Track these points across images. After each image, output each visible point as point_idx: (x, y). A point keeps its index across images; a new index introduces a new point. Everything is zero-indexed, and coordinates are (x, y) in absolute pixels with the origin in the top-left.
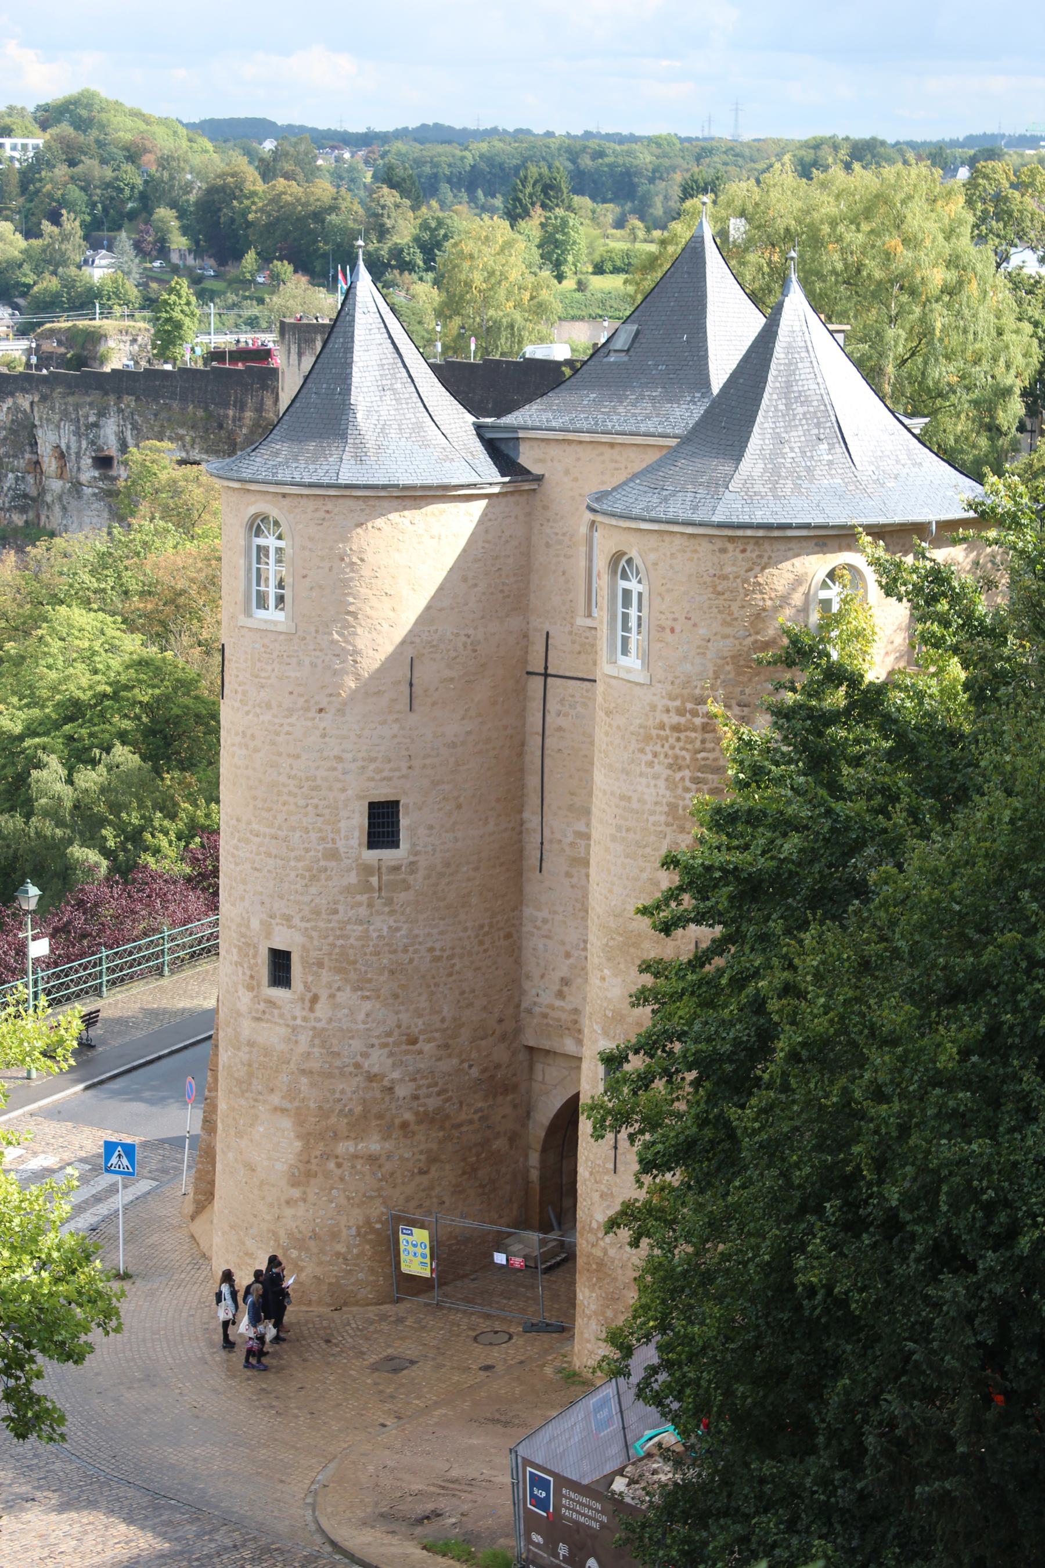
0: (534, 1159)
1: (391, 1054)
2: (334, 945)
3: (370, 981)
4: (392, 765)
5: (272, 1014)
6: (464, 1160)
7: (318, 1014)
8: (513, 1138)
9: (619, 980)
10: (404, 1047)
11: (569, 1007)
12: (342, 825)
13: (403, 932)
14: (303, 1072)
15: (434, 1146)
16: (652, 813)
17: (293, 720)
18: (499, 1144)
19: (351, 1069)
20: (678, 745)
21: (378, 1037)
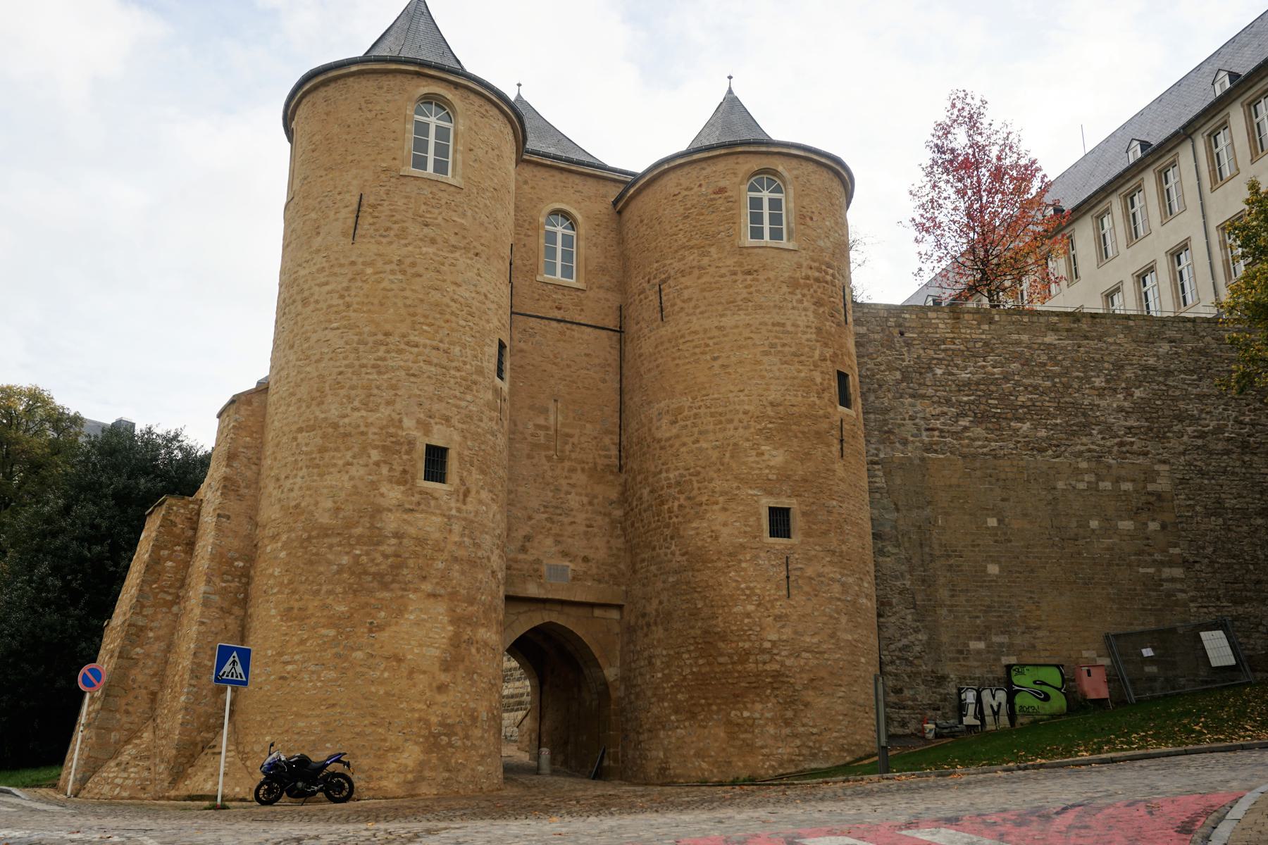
5: (428, 505)
11: (531, 558)
14: (456, 559)
16: (805, 333)
17: (457, 255)
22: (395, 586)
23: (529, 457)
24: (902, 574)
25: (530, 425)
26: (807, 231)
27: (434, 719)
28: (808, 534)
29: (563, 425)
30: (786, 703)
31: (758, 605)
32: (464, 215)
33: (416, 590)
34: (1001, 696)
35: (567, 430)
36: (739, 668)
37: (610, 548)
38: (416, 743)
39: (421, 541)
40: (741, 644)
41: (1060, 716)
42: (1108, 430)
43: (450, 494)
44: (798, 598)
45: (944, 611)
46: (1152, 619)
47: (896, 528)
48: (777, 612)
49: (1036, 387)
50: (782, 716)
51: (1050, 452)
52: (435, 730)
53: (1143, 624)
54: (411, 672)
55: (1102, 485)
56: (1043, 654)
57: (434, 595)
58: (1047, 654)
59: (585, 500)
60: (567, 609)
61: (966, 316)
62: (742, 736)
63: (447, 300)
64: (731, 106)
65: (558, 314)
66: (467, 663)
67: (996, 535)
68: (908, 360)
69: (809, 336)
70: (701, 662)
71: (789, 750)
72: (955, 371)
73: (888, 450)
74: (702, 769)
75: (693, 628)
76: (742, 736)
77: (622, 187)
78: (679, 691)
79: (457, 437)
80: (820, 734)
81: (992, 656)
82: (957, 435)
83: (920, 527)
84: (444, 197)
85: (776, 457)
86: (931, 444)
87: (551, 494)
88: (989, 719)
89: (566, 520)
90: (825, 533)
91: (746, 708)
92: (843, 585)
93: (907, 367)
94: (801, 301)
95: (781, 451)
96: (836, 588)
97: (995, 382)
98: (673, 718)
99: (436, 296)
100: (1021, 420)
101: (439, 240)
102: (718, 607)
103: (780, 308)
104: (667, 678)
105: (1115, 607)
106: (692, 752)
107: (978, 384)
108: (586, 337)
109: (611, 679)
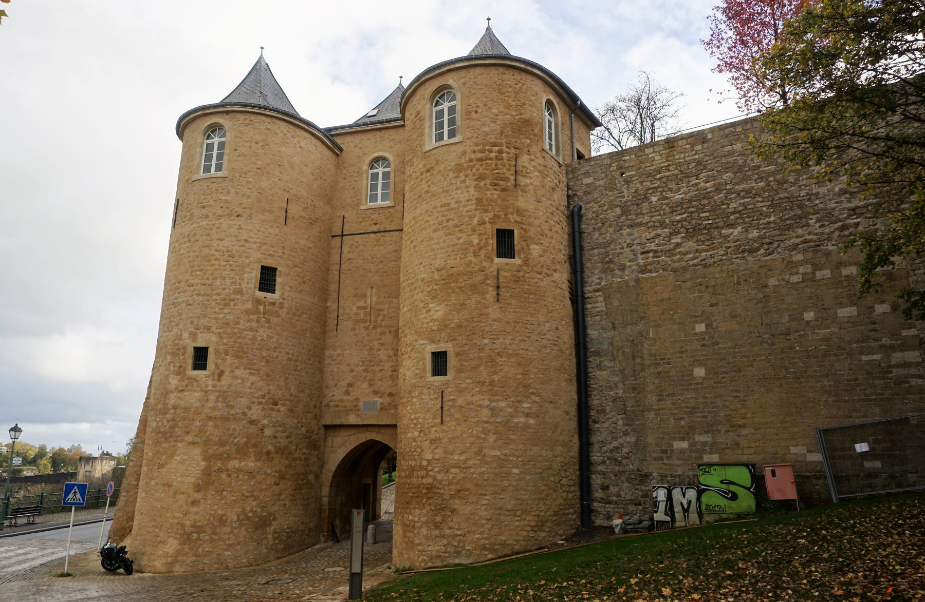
0: (325, 491)
1: (263, 410)
2: (235, 342)
3: (254, 364)
4: (274, 249)
6: (296, 481)
7: (223, 382)
8: (317, 477)
9: (443, 306)
10: (271, 406)
12: (246, 275)
13: (274, 340)
14: (210, 418)
15: (283, 469)
16: (465, 206)
17: (222, 221)
18: (311, 477)
19: (240, 416)
20: (481, 168)
21: (257, 398)
22: (172, 439)
23: (353, 329)
24: (616, 385)
25: (354, 308)
26: (472, 123)
27: (188, 523)
28: (459, 371)
29: (377, 303)
30: (436, 510)
31: (421, 432)
32: (228, 193)
33: (182, 441)
34: (692, 494)
35: (379, 307)
36: (409, 481)
38: (175, 538)
39: (186, 410)
41: (747, 515)
42: (828, 216)
43: (208, 376)
44: (450, 424)
45: (652, 415)
46: (877, 410)
47: (612, 344)
48: (432, 436)
49: (748, 192)
50: (433, 521)
51: (762, 251)
52: (188, 530)
53: (865, 416)
54: (175, 494)
55: (819, 274)
56: (747, 451)
57: (193, 443)
58: (752, 451)
59: (391, 353)
60: (383, 430)
61: (680, 143)
63: (213, 252)
64: (260, 73)
65: (375, 229)
66: (217, 485)
67: (704, 339)
68: (627, 195)
69: (469, 208)
71: (437, 548)
72: (669, 195)
73: (609, 277)
77: (335, 139)
79: (214, 339)
80: (464, 535)
81: (694, 455)
82: (670, 253)
83: (633, 341)
84: (215, 186)
85: (438, 311)
86: (645, 265)
87: (366, 353)
88: (679, 516)
89: (377, 369)
90: (475, 368)
91: (411, 513)
92: (492, 409)
93: (626, 202)
94: (464, 181)
95: (443, 306)
96: (485, 412)
97: (707, 196)
99: (206, 250)
100: (733, 226)
101: (210, 214)
103: (447, 191)
105: (831, 399)
107: (690, 201)
108: (394, 239)
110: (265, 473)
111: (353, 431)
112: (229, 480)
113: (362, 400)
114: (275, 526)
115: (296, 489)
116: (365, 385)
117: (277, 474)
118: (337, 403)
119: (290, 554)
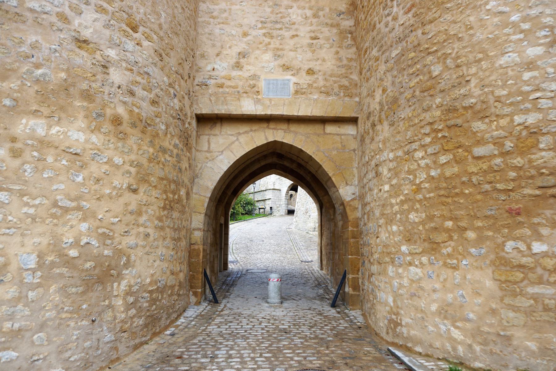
1: (107, 26)
6: (165, 192)
15: (145, 162)
36: (518, 161)
37: (340, 59)
40: (518, 119)
59: (309, 13)
60: (294, 127)
62: (531, 290)
70: (443, 159)
74: (452, 339)
75: (428, 109)
76: (531, 290)
78: (412, 209)
87: (269, 10)
89: (287, 34)
91: (539, 238)
98: (404, 248)
102: (468, 65)
104: (396, 190)
106: (434, 307)
109: (348, 199)
110: (110, 161)
111: (243, 128)
112: (17, 163)
113: (262, 77)
114: (129, 279)
115: (164, 208)
116: (268, 56)
117: (133, 170)
118: (220, 81)
119: (155, 334)
